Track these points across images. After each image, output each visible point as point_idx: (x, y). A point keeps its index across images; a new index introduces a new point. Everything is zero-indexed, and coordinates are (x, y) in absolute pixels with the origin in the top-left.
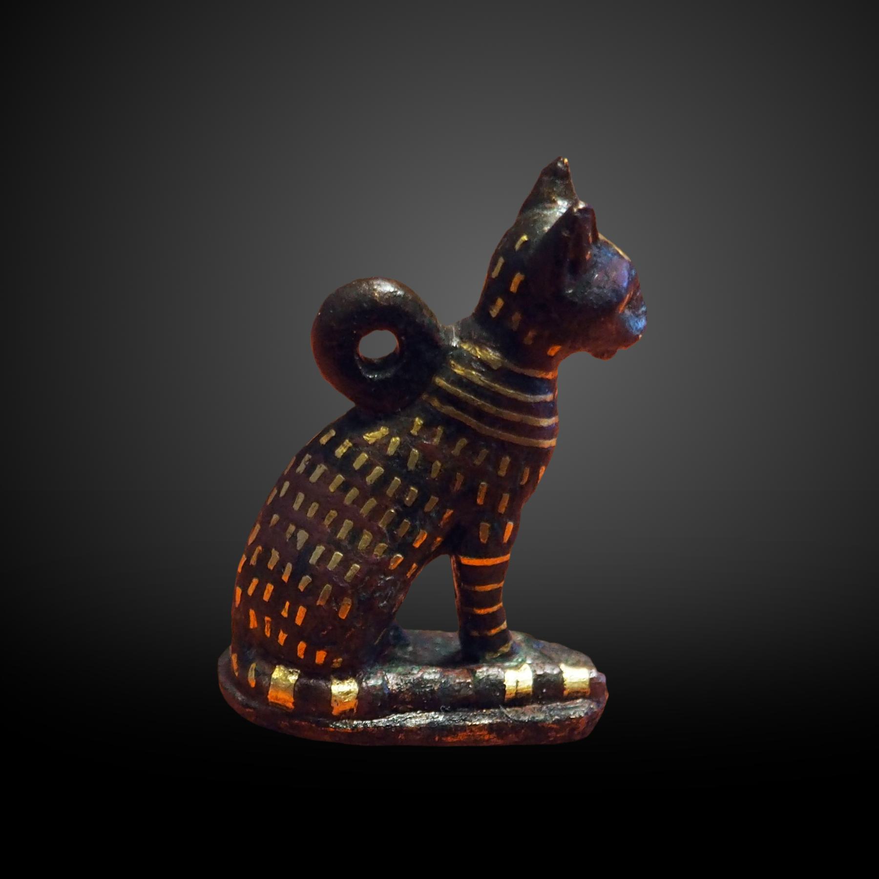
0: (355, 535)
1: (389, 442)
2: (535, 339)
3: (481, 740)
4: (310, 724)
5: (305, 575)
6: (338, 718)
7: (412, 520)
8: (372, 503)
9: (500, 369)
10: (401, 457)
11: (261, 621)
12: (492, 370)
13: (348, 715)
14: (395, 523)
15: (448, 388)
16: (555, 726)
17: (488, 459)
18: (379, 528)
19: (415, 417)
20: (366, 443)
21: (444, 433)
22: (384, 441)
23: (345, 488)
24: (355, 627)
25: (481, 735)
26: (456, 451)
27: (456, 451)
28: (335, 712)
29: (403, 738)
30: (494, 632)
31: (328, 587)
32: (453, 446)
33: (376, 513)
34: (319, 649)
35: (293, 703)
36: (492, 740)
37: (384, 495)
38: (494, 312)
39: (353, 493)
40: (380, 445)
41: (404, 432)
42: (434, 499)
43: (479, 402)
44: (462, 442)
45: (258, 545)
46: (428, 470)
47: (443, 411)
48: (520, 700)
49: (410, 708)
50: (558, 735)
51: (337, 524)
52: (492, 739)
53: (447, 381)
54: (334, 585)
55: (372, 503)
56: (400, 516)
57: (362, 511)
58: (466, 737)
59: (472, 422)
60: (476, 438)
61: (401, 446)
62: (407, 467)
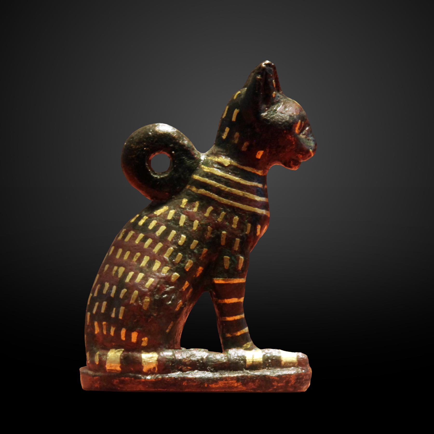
0: (151, 263)
1: (168, 213)
2: (249, 147)
3: (233, 386)
4: (130, 378)
5: (123, 289)
6: (147, 374)
7: (184, 253)
8: (160, 246)
9: (229, 166)
10: (176, 220)
11: (101, 327)
12: (225, 167)
14: (173, 255)
15: (200, 179)
16: (277, 378)
17: (225, 218)
19: (183, 198)
20: (156, 216)
21: (200, 205)
22: (166, 213)
23: (144, 240)
24: (153, 316)
25: (232, 383)
26: (207, 215)
27: (207, 215)
28: (145, 370)
29: (186, 384)
30: (239, 334)
31: (136, 292)
32: (205, 212)
33: (163, 250)
34: (133, 331)
35: (121, 367)
36: (239, 387)
37: (166, 240)
38: (224, 137)
39: (149, 242)
40: (163, 215)
41: (177, 206)
42: (195, 242)
43: (218, 185)
44: (210, 209)
45: (98, 284)
46: (192, 226)
47: (199, 192)
49: (189, 369)
50: (279, 385)
51: (140, 260)
52: (238, 386)
53: (200, 176)
54: (140, 290)
55: (160, 246)
56: (175, 252)
57: (154, 250)
58: (223, 385)
59: (216, 196)
60: (218, 206)
61: (175, 214)
62: (179, 225)
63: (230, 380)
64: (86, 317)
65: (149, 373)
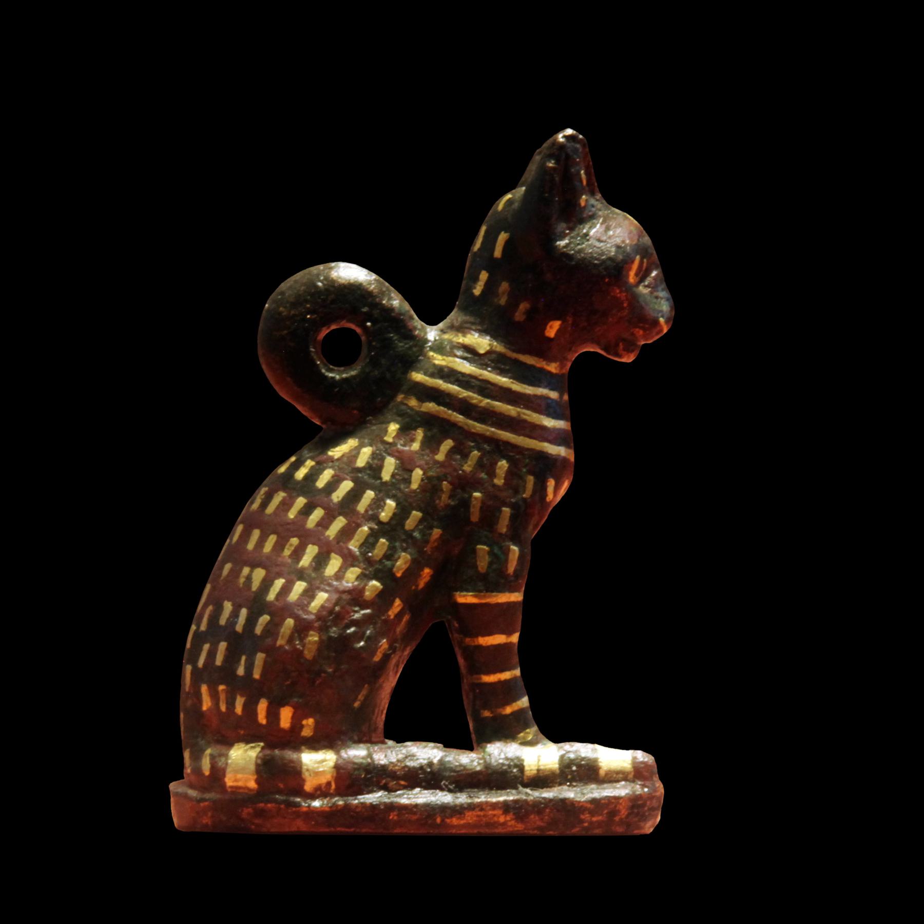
0: (321, 561)
1: (358, 453)
2: (529, 313)
3: (495, 822)
4: (277, 805)
5: (261, 615)
6: (312, 796)
7: (391, 539)
8: (340, 523)
9: (488, 353)
10: (374, 468)
11: (214, 696)
12: (480, 355)
13: (321, 793)
14: (369, 543)
15: (427, 381)
16: (589, 806)
17: (480, 465)
18: (350, 551)
19: (389, 422)
20: (332, 459)
21: (425, 437)
22: (354, 453)
23: (307, 511)
24: (325, 672)
25: (494, 815)
26: (440, 457)
27: (440, 457)
28: (308, 787)
29: (395, 818)
30: (508, 710)
31: (290, 622)
32: (436, 450)
33: (347, 533)
34: (283, 706)
35: (257, 781)
36: (510, 824)
37: (354, 512)
39: (317, 514)
40: (348, 457)
42: (416, 514)
43: (464, 393)
44: (448, 444)
45: (209, 605)
46: (408, 481)
47: (423, 409)
48: (542, 780)
49: (403, 785)
50: (594, 819)
51: (298, 553)
52: (508, 821)
53: (425, 374)
54: (297, 618)
55: (340, 523)
56: (373, 537)
57: (328, 533)
58: (475, 819)
59: (459, 418)
60: (464, 439)
61: (374, 456)
62: (381, 478)
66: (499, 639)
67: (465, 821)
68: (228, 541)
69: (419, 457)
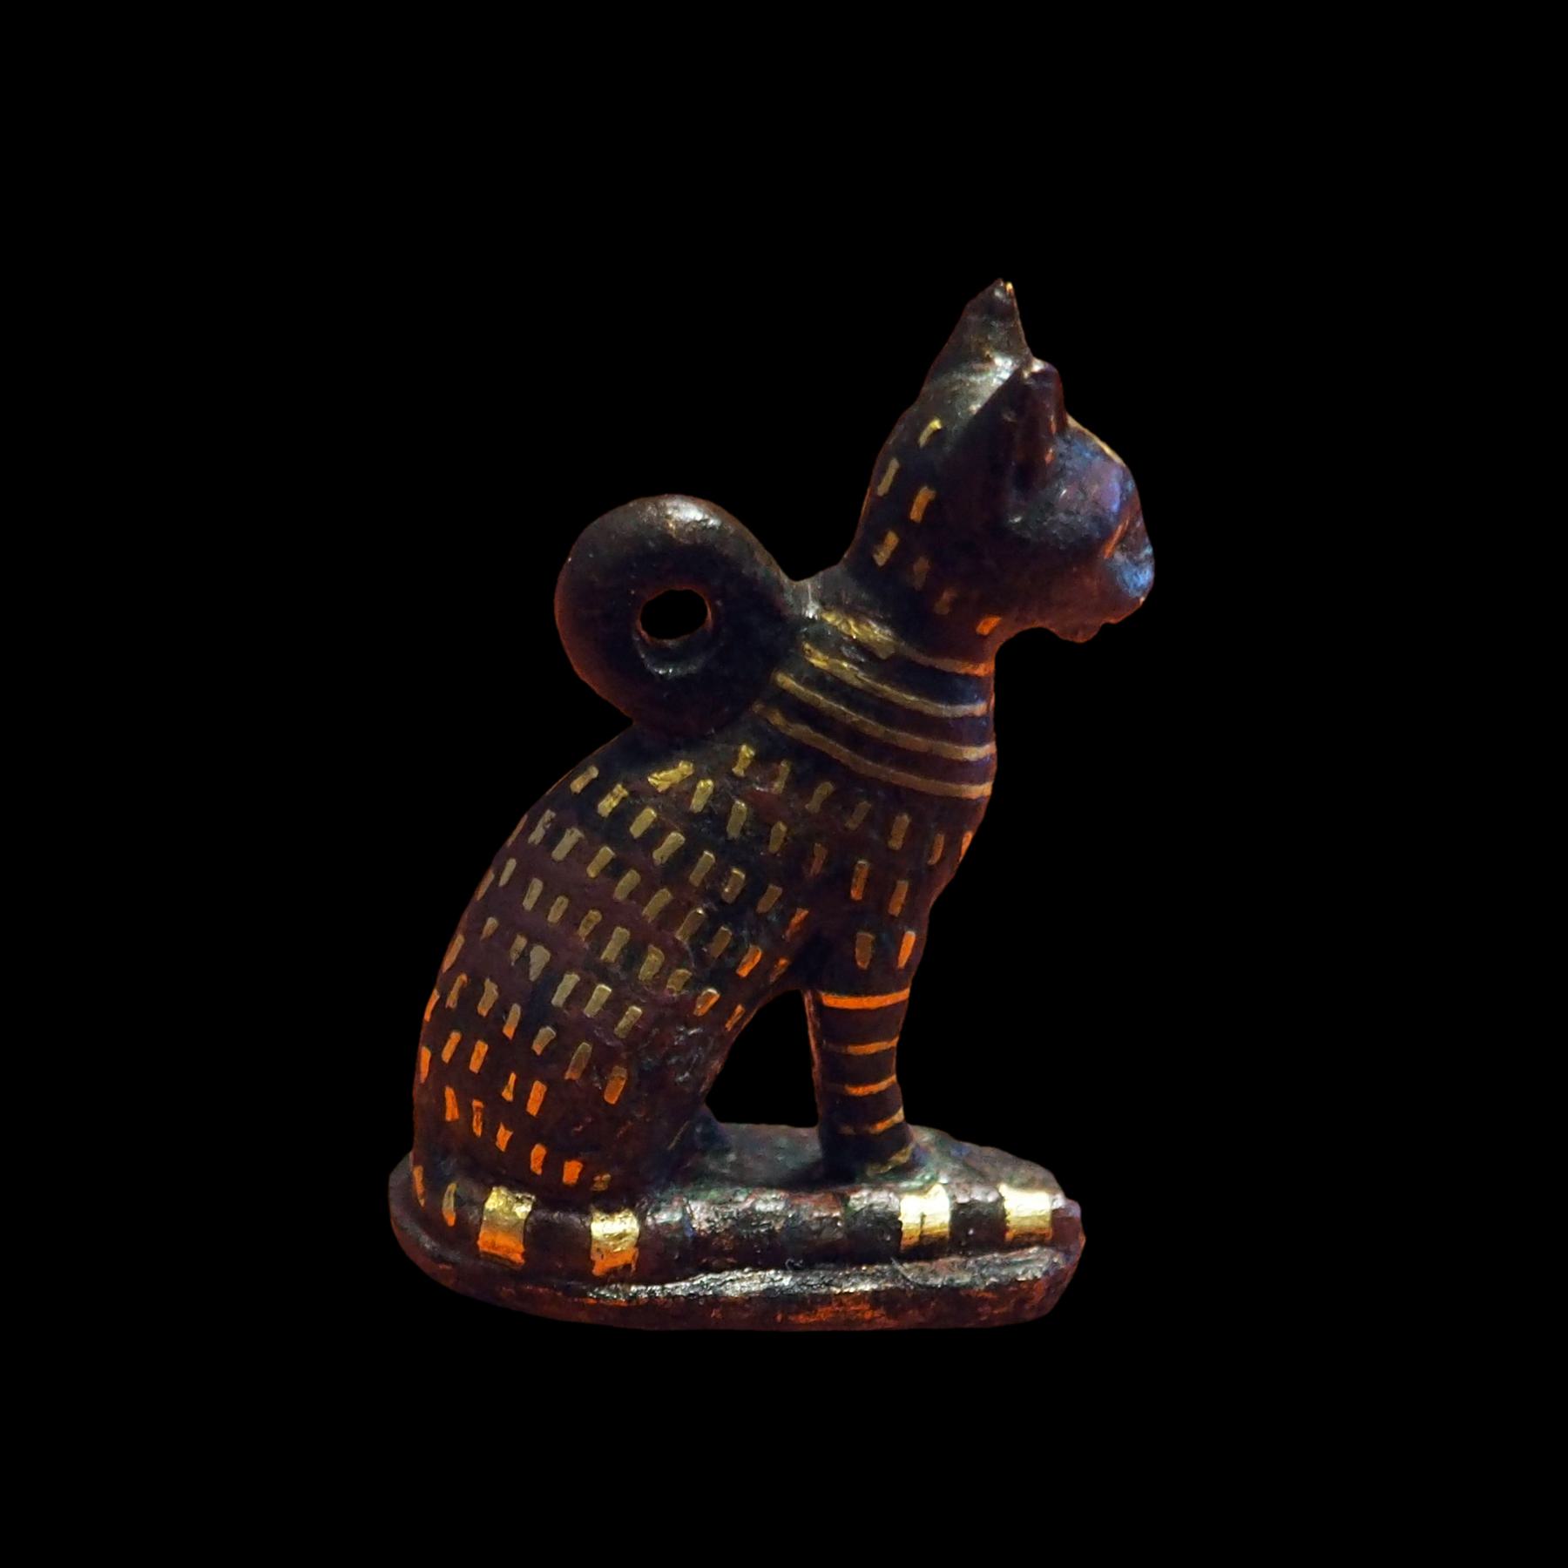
0: (633, 954)
1: (694, 788)
2: (955, 604)
3: (857, 1319)
4: (552, 1291)
5: (544, 1025)
6: (603, 1282)
7: (736, 927)
8: (663, 897)
9: (892, 659)
10: (716, 815)
11: (465, 1109)
12: (878, 660)
14: (705, 933)
15: (799, 691)
16: (990, 1295)
17: (870, 819)
19: (741, 745)
20: (653, 790)
21: (793, 772)
22: (685, 787)
23: (615, 870)
24: (633, 1118)
25: (857, 1311)
26: (813, 805)
27: (813, 805)
28: (597, 1271)
30: (880, 1127)
31: (585, 1047)
32: (808, 795)
33: (671, 916)
34: (570, 1159)
35: (523, 1255)
36: (878, 1321)
37: (685, 883)
39: (630, 879)
40: (678, 793)
42: (775, 891)
43: (855, 717)
44: (825, 789)
45: (460, 972)
46: (764, 839)
47: (791, 732)
49: (732, 1264)
50: (996, 1312)
51: (600, 935)
52: (877, 1318)
53: (797, 679)
54: (597, 1043)
55: (663, 897)
56: (713, 920)
57: (645, 911)
58: (831, 1315)
59: (842, 753)
60: (848, 782)
61: (716, 795)
62: (726, 834)
63: (852, 1305)
64: (417, 1064)
65: (609, 1280)
66: (873, 1048)
67: (815, 1319)
68: (490, 877)
69: (863, 1314)
